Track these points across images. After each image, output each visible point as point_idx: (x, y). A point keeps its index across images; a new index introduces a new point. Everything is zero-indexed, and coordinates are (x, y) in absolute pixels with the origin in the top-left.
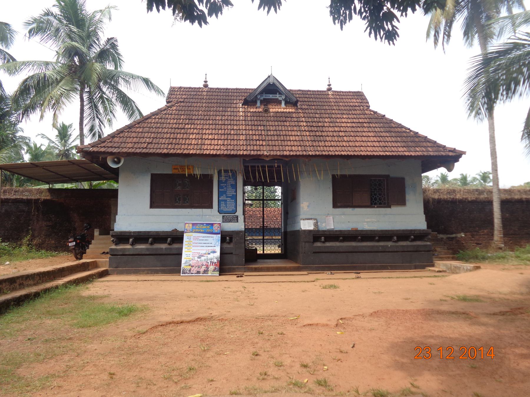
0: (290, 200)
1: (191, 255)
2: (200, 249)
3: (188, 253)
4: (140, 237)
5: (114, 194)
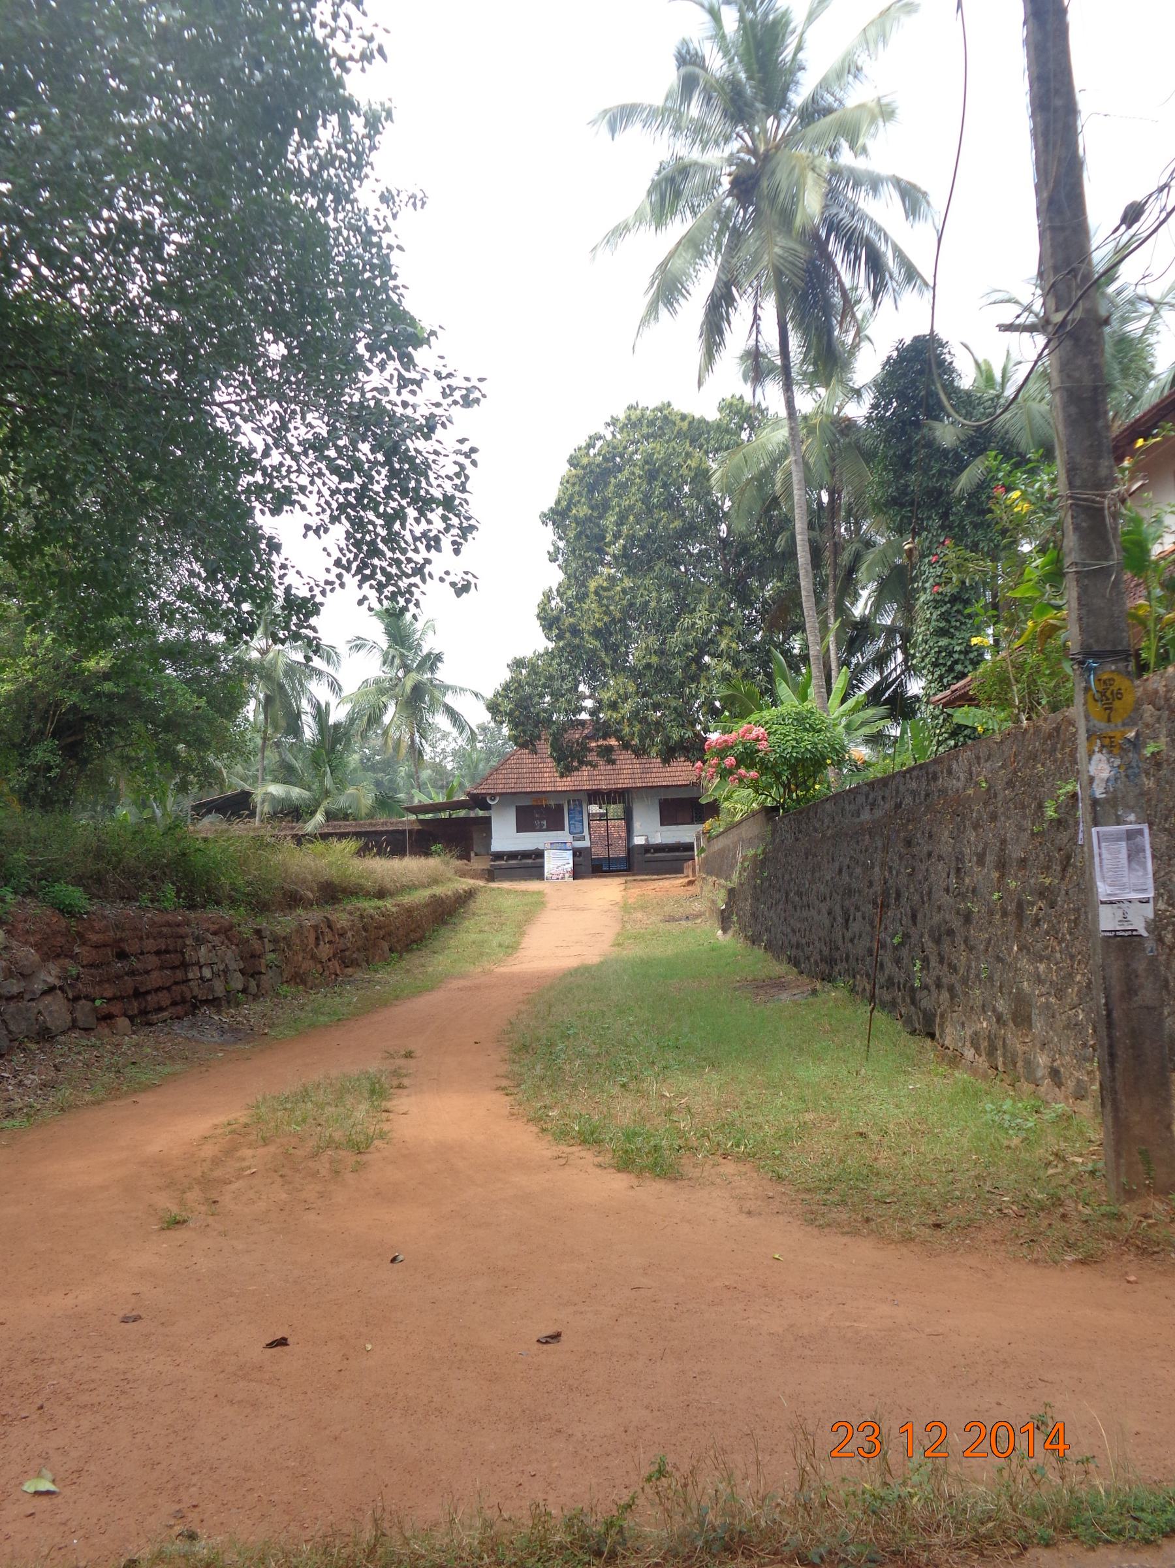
0: (628, 818)
2: (558, 862)
4: (512, 855)
5: (487, 821)
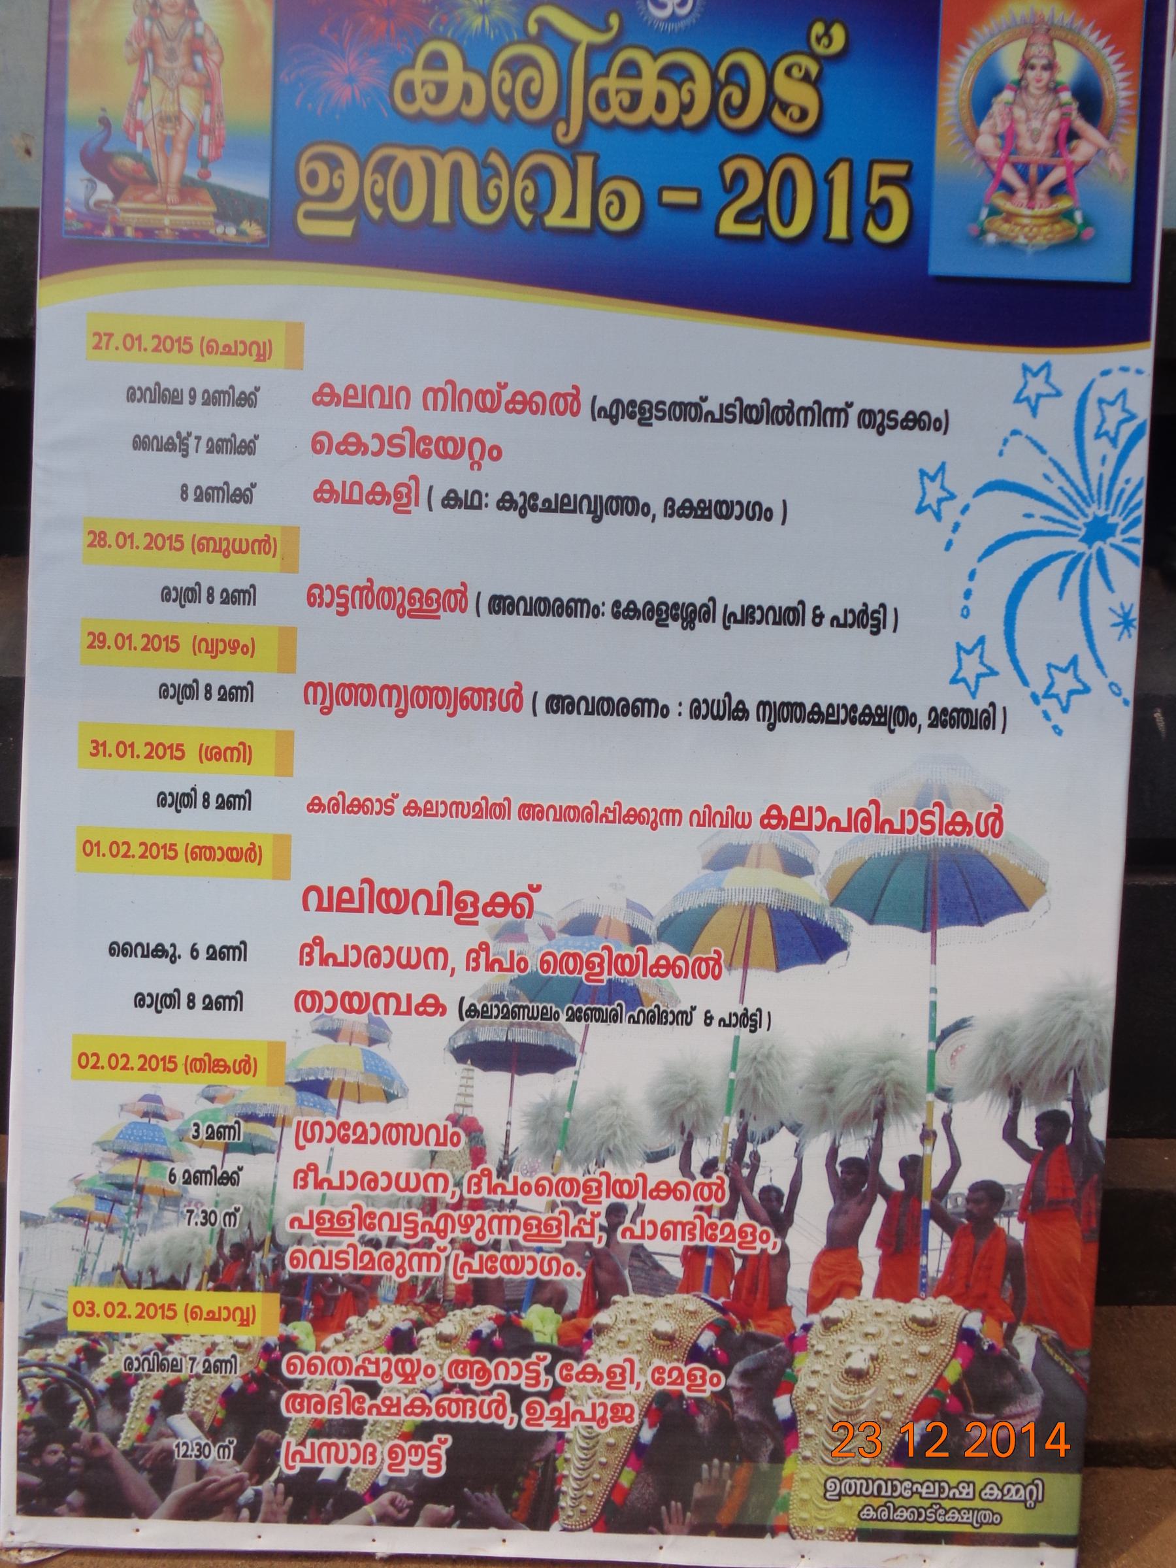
1: (271, 982)
3: (192, 903)
